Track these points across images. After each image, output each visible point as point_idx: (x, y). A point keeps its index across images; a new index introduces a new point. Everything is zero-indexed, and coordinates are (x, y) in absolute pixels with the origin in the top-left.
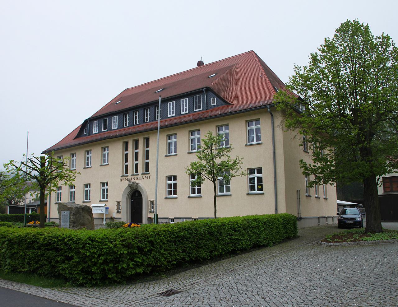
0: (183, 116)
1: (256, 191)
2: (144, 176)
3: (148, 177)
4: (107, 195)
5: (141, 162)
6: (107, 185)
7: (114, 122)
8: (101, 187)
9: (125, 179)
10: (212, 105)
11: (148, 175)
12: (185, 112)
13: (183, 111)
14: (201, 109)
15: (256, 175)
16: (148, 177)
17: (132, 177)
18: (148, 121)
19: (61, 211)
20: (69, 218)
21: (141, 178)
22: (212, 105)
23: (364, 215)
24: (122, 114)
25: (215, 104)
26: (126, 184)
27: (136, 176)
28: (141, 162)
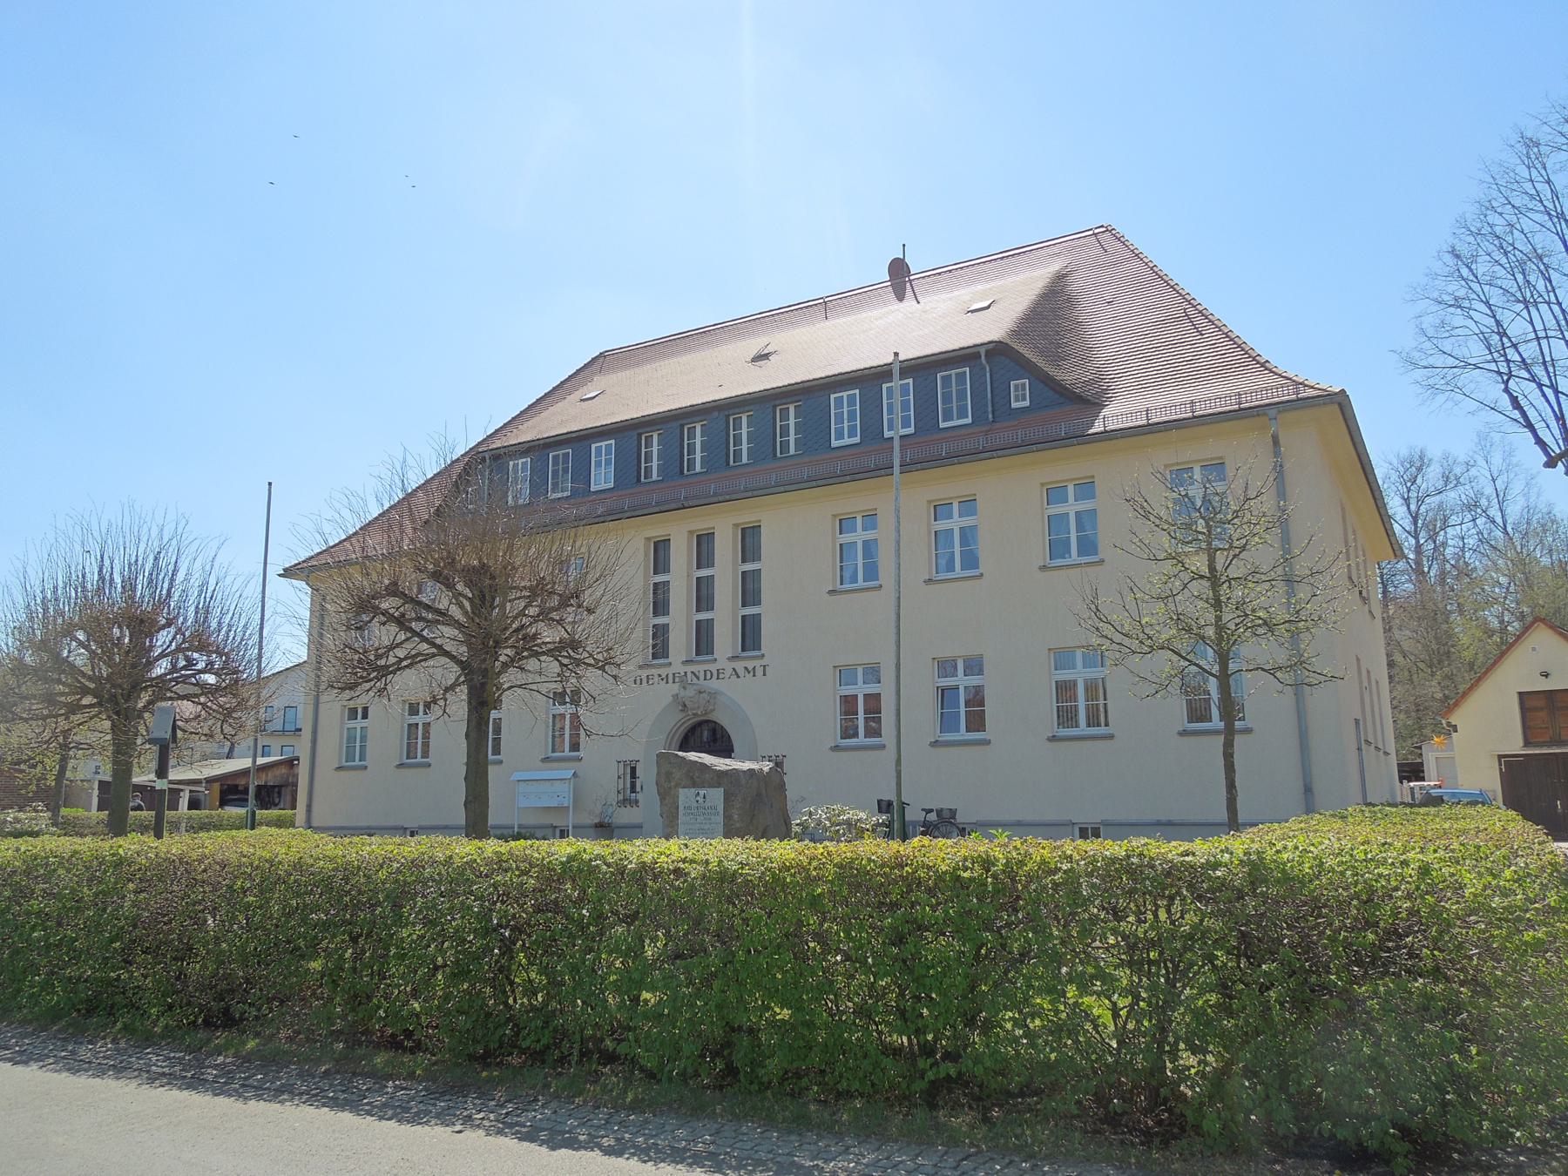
0: (839, 453)
1: (861, 739)
2: (739, 666)
3: (759, 671)
4: (426, 745)
5: (725, 617)
6: (365, 716)
7: (598, 464)
8: (342, 723)
9: (656, 679)
10: (1014, 405)
11: (757, 663)
12: (847, 441)
13: (840, 436)
14: (969, 420)
15: (962, 681)
16: (759, 671)
17: (689, 669)
18: (745, 460)
19: (677, 786)
20: (720, 819)
21: (729, 671)
22: (1014, 405)
23: (477, 827)
24: (635, 433)
25: (1027, 403)
26: (662, 695)
27: (706, 667)
28: (725, 617)
